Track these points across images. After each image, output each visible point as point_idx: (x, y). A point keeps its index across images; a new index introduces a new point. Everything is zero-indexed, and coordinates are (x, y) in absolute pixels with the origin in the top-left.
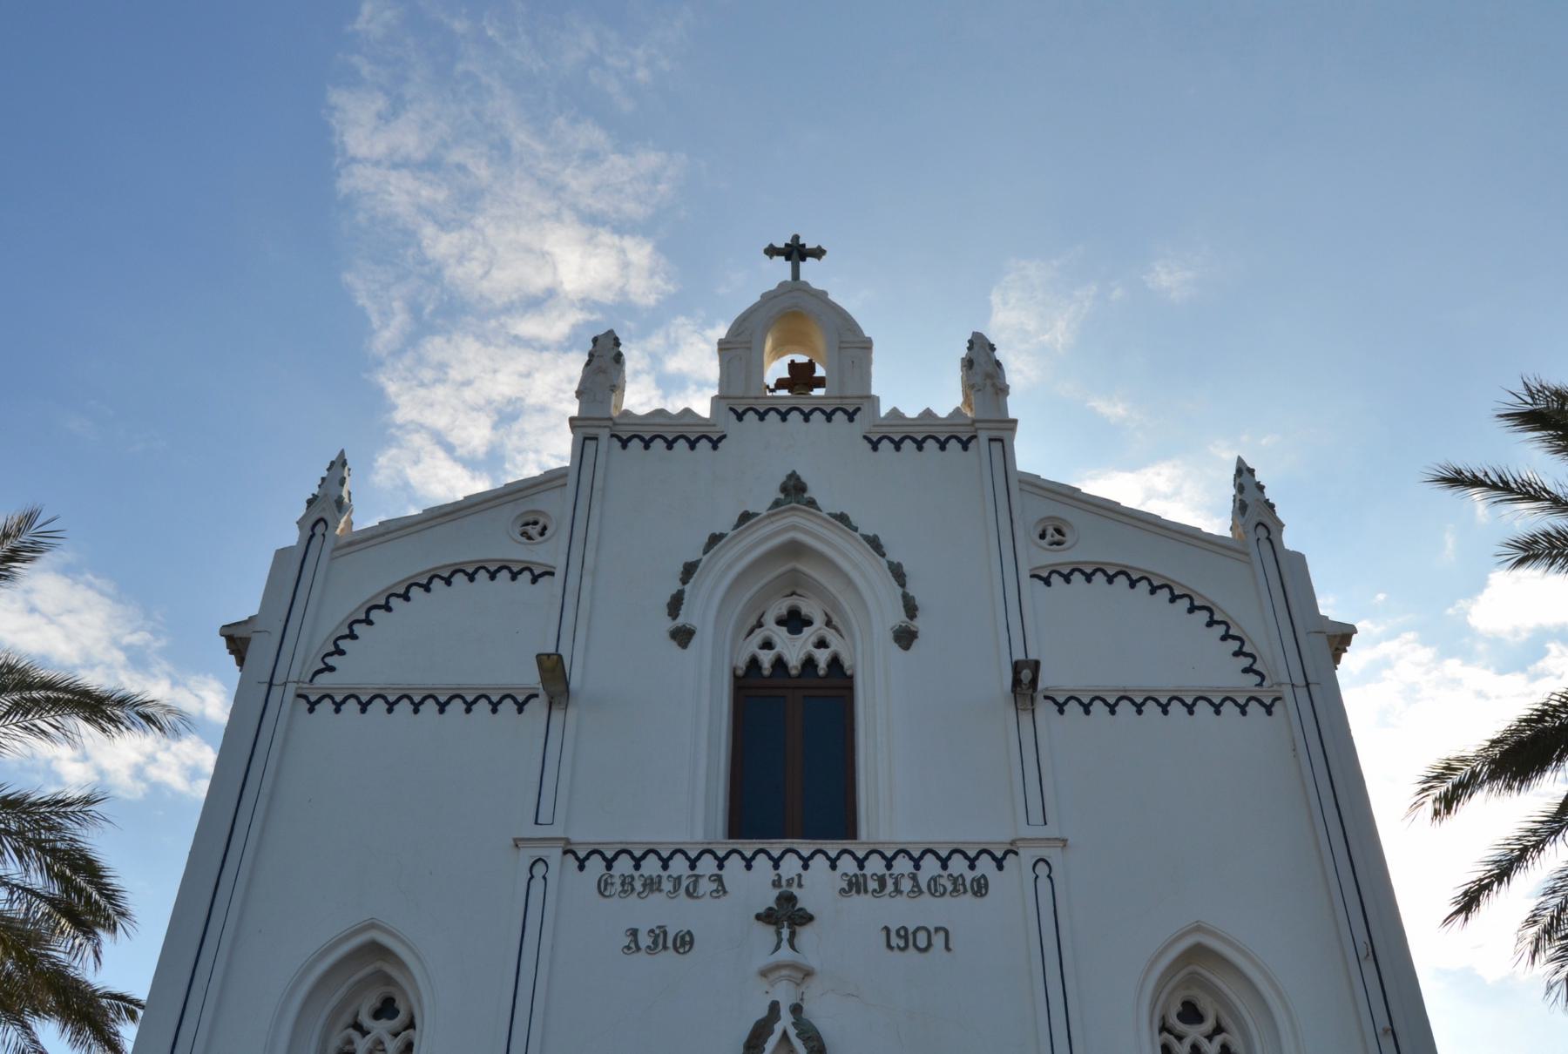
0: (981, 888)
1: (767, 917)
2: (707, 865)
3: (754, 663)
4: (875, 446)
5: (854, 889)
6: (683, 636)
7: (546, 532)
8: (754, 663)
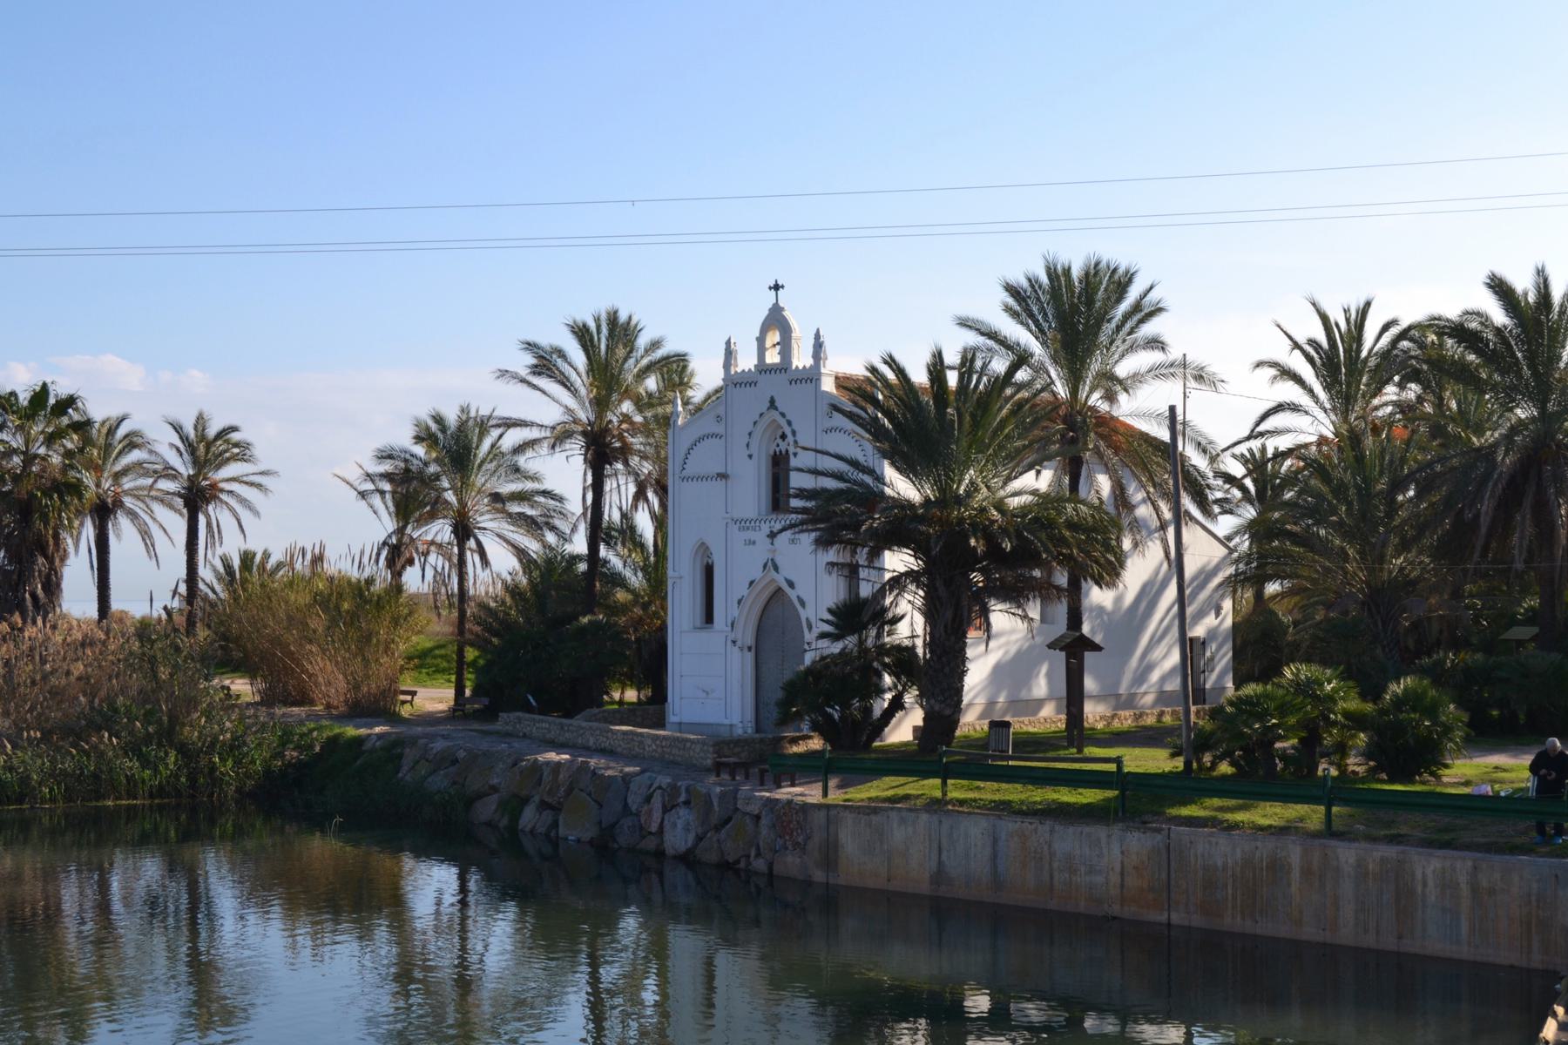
2: (757, 524)
3: (775, 452)
6: (750, 456)
7: (716, 983)
8: (775, 452)
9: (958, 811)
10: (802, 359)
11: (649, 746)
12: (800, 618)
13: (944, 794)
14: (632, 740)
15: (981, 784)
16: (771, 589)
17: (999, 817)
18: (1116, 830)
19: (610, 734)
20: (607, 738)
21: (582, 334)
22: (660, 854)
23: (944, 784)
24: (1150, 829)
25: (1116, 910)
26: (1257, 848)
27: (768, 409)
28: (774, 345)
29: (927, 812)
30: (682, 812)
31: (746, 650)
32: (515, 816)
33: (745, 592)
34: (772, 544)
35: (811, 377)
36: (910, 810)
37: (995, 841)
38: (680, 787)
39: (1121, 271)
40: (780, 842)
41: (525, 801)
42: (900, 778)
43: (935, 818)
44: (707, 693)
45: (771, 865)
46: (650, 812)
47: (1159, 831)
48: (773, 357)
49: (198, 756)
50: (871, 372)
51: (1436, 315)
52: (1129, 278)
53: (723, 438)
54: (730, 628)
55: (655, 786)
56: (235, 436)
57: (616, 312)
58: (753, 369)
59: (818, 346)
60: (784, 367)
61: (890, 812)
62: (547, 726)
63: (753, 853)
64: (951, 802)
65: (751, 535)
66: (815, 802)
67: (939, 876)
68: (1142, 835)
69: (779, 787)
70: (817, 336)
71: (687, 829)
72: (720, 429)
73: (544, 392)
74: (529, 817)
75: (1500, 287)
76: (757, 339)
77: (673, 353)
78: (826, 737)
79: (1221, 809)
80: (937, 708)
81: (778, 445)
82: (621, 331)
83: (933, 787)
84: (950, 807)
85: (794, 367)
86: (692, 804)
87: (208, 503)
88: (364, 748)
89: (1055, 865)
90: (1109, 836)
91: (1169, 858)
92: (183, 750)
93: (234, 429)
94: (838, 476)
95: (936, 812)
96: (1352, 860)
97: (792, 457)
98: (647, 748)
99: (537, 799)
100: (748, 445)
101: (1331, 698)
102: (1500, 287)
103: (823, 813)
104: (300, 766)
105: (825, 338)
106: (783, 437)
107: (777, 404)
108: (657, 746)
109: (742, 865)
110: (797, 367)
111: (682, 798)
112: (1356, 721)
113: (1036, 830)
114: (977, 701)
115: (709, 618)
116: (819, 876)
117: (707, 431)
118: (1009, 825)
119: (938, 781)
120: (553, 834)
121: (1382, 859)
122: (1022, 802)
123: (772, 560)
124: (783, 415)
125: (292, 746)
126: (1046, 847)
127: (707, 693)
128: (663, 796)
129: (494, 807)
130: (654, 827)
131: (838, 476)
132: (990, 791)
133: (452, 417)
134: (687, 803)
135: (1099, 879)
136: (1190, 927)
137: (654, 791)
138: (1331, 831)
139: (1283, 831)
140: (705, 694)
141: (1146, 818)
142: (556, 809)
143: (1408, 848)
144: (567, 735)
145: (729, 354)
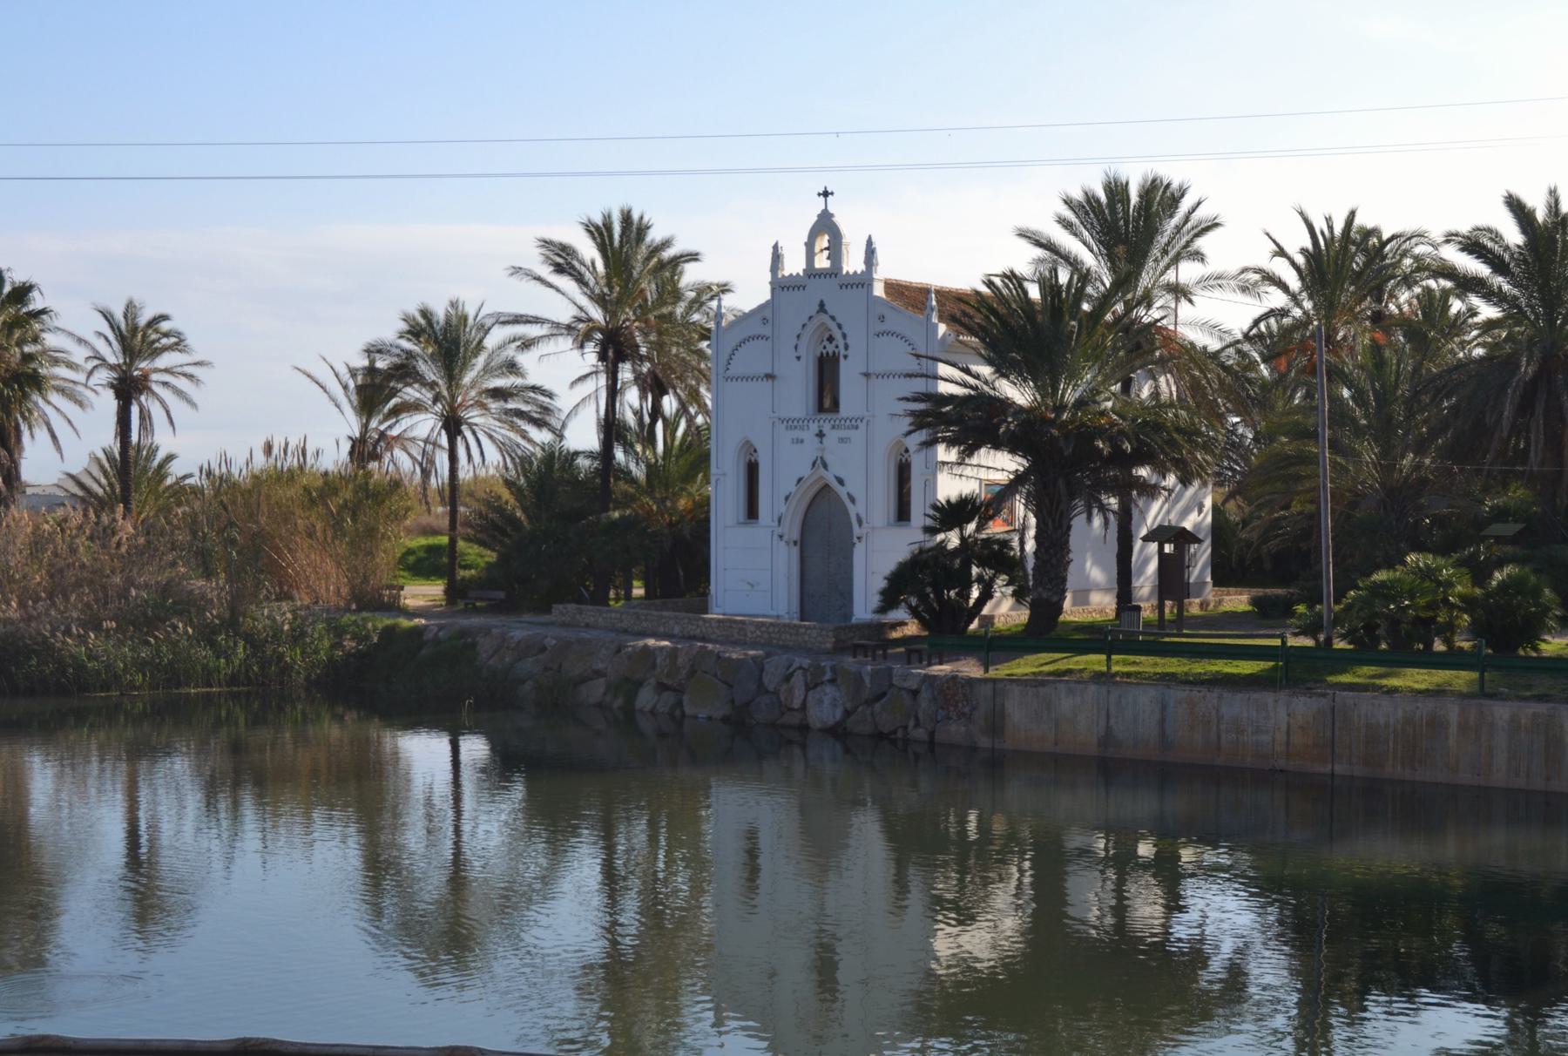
0: (857, 428)
1: (817, 435)
2: (806, 422)
3: (822, 354)
4: (841, 287)
5: (1134, 199)
6: (798, 358)
7: (761, 861)
8: (822, 354)
9: (1126, 682)
10: (853, 263)
11: (752, 633)
12: (848, 514)
13: (1109, 667)
14: (731, 627)
15: (1143, 658)
16: (821, 484)
17: (1169, 687)
18: (1283, 696)
19: (701, 623)
20: (698, 626)
21: (600, 233)
22: (804, 728)
23: (1109, 659)
24: (1315, 694)
25: (1281, 763)
26: (1417, 708)
27: (818, 312)
28: (822, 251)
29: (1095, 683)
30: (829, 689)
31: (792, 543)
32: (631, 698)
33: (793, 489)
34: (821, 442)
35: (863, 282)
36: (1078, 682)
37: (1164, 708)
38: (824, 667)
39: (1175, 185)
40: (942, 713)
41: (640, 684)
42: (1051, 655)
43: (1104, 689)
44: (752, 586)
45: (932, 734)
46: (791, 691)
47: (1324, 695)
48: (822, 262)
49: (264, 646)
50: (989, 287)
51: (1454, 231)
52: (1183, 192)
53: (770, 340)
54: (777, 523)
55: (794, 667)
56: (165, 326)
57: (629, 212)
58: (801, 274)
59: (870, 252)
60: (834, 271)
61: (1057, 685)
62: (618, 616)
63: (911, 723)
64: (1117, 674)
65: (798, 434)
66: (978, 676)
67: (1107, 739)
68: (1308, 700)
69: (930, 664)
70: (869, 242)
71: (834, 704)
72: (766, 331)
73: (558, 290)
74: (645, 698)
75: (1516, 207)
76: (806, 244)
77: (686, 252)
78: (924, 623)
79: (1374, 677)
80: (1045, 596)
81: (825, 348)
82: (634, 229)
83: (1099, 662)
84: (1118, 679)
85: (844, 272)
86: (839, 681)
87: (141, 393)
88: (425, 638)
89: (1223, 727)
90: (1276, 701)
91: (1333, 718)
92: (251, 640)
93: (164, 318)
94: (965, 385)
95: (1104, 683)
96: (1506, 716)
97: (842, 358)
98: (749, 634)
99: (652, 681)
100: (796, 347)
101: (1449, 584)
102: (1516, 207)
103: (990, 686)
104: (359, 655)
105: (877, 244)
106: (831, 339)
107: (826, 308)
108: (762, 632)
109: (900, 734)
110: (848, 272)
111: (828, 676)
112: (1469, 603)
113: (1204, 697)
114: (1147, 584)
115: (752, 512)
116: (984, 742)
117: (751, 333)
118: (1177, 694)
119: (1104, 657)
120: (678, 713)
121: (1534, 714)
122: (1186, 674)
123: (821, 458)
124: (833, 318)
125: (348, 637)
126: (1214, 712)
127: (752, 586)
128: (805, 676)
129: (602, 690)
130: (797, 704)
131: (965, 385)
132: (1148, 664)
133: (440, 312)
134: (832, 681)
135: (1265, 738)
136: (1352, 776)
137: (794, 671)
138: (1483, 692)
139: (1438, 692)
140: (749, 587)
141: (1309, 685)
142: (679, 691)
143: (1557, 705)
144: (645, 624)
145: (777, 257)
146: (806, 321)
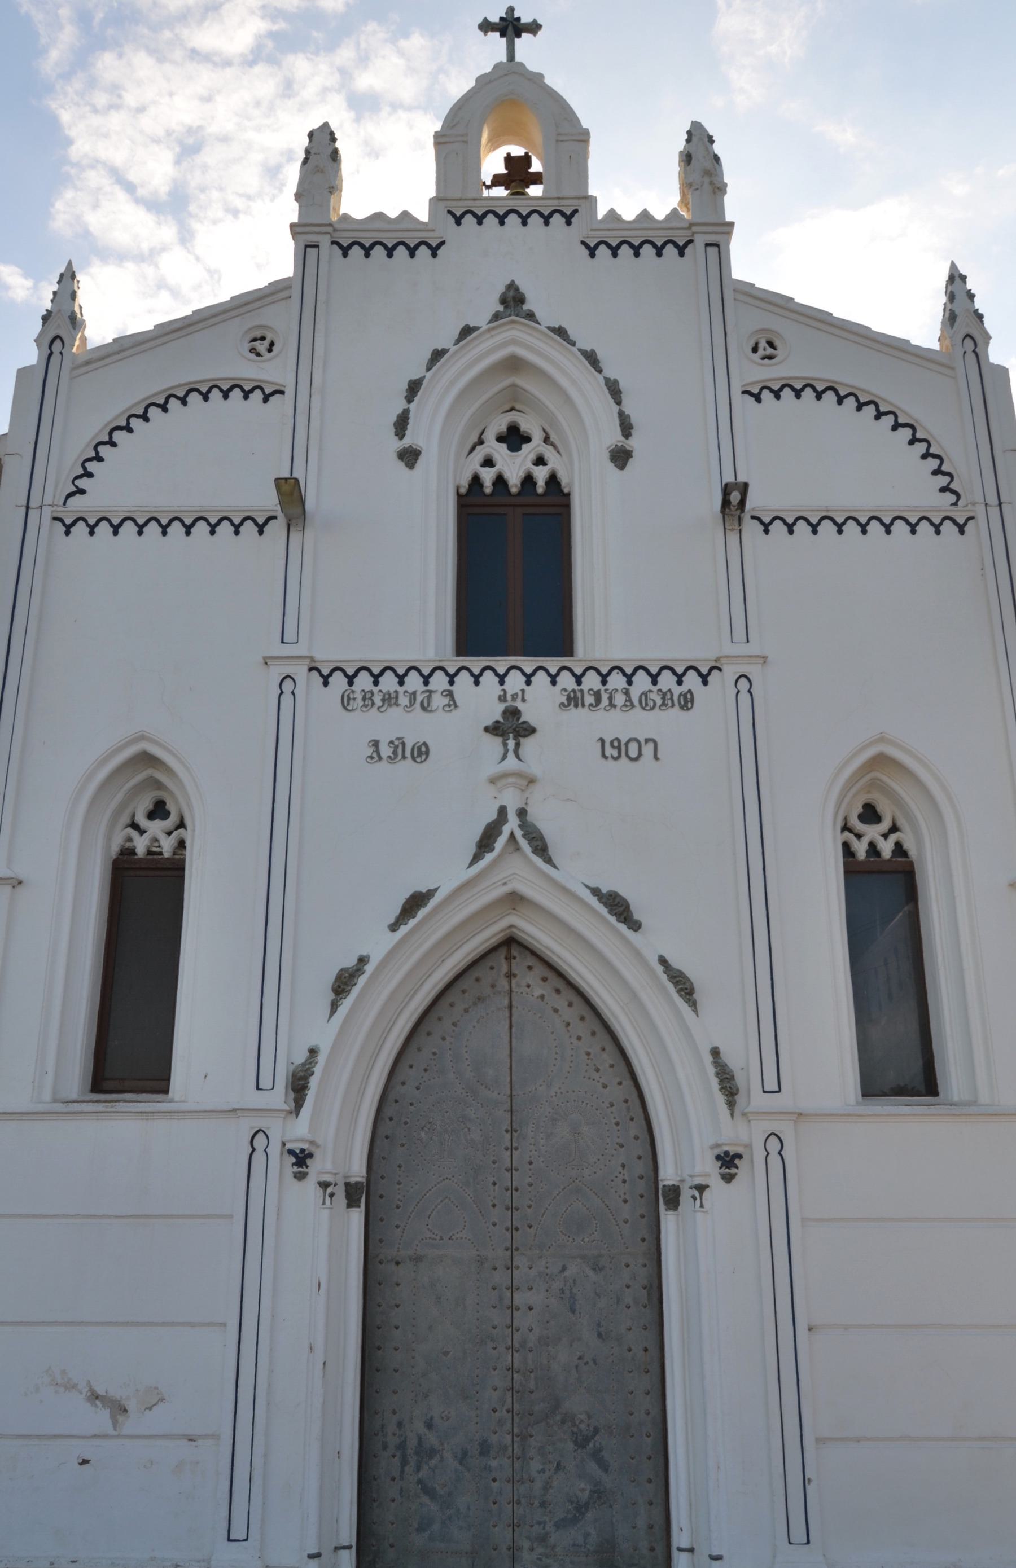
0: (687, 702)
1: (495, 729)
2: (440, 681)
4: (592, 253)
6: (410, 457)
31: (340, 1192)
44: (119, 1409)
85: (601, 212)
110: (612, 214)
146: (445, 339)
